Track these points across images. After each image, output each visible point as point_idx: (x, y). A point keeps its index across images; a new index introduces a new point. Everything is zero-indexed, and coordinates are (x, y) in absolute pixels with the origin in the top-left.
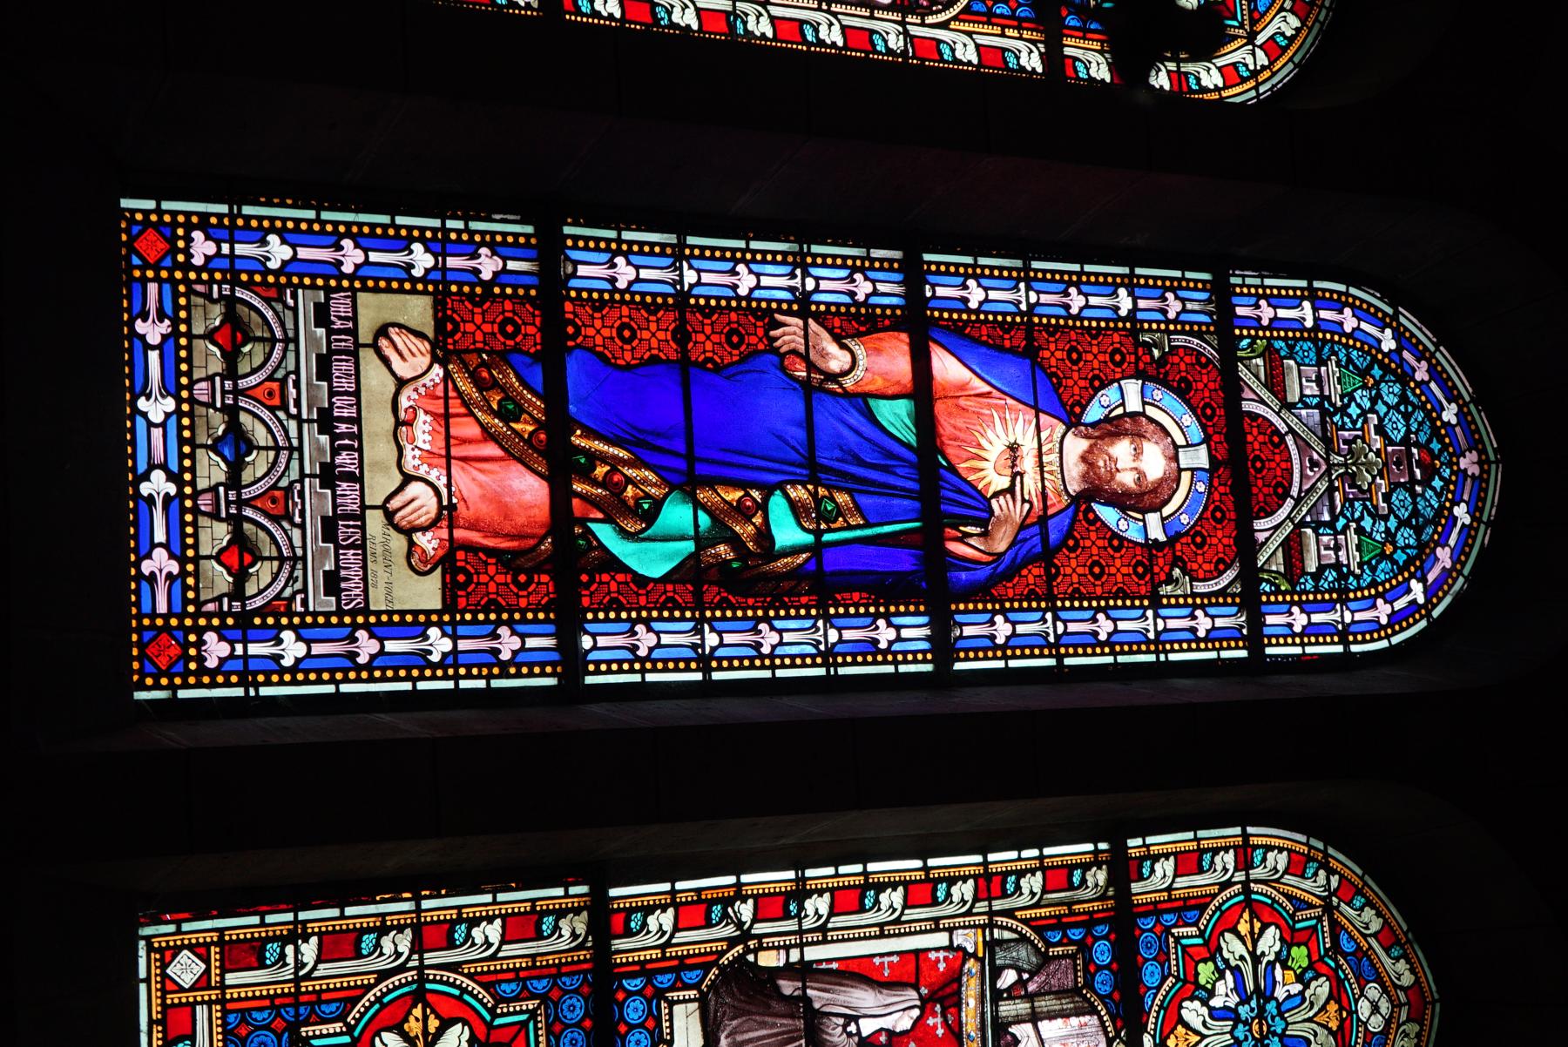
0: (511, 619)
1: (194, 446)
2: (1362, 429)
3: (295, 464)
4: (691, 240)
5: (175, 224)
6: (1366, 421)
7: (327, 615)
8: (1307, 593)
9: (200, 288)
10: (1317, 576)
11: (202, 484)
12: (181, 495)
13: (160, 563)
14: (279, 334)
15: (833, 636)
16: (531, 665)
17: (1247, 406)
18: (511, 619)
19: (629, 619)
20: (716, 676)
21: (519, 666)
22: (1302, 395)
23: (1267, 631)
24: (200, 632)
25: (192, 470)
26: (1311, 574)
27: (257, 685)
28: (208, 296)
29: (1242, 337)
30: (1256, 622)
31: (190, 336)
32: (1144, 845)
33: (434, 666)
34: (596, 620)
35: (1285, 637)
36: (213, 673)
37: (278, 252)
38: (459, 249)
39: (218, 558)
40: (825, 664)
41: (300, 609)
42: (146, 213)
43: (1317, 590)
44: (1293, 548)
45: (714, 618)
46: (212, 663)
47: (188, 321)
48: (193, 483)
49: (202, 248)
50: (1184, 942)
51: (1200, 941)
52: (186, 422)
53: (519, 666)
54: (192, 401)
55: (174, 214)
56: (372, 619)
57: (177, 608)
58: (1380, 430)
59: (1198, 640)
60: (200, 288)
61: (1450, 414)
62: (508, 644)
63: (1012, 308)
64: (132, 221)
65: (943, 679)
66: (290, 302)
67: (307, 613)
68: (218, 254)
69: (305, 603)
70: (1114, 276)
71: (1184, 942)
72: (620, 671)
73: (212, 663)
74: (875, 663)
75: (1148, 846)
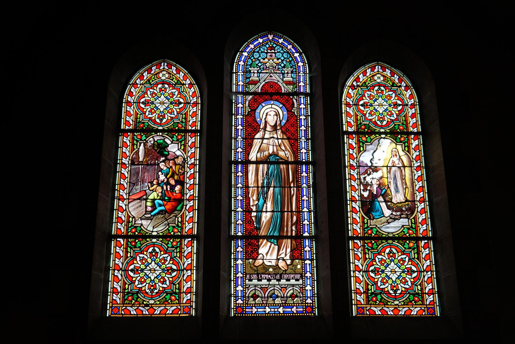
0: (302, 221)
1: (274, 303)
2: (264, 63)
3: (277, 286)
4: (233, 209)
5: (236, 306)
6: (262, 62)
7: (303, 281)
8: (296, 81)
9: (247, 302)
10: (293, 78)
11: (281, 302)
12: (283, 306)
13: (294, 309)
14: (254, 288)
15: (303, 138)
16: (309, 206)
17: (260, 91)
18: (302, 221)
19: (303, 252)
20: (309, 114)
21: (309, 208)
22: (257, 77)
23: (304, 92)
24: (306, 303)
25: (278, 304)
26: (293, 80)
27: (310, 185)
28: (248, 301)
29: (246, 90)
30: (302, 94)
31: (255, 304)
32: (350, 212)
33: (308, 175)
34: (300, 159)
35: (306, 110)
36: (313, 301)
37: (240, 288)
38: (237, 256)
39: (293, 300)
40: (310, 188)
41: (302, 286)
42: (234, 311)
43: (296, 78)
44: (288, 83)
45: (302, 209)
46: (311, 302)
47: (252, 304)
48: (280, 304)
49: (240, 301)
50: (364, 120)
51: (363, 117)
52: (270, 305)
53: (309, 208)
54: (266, 304)
55: (234, 306)
56: (303, 273)
57: (302, 307)
58: (264, 59)
59: (306, 108)
60: (247, 302)
61: (261, 40)
62: (307, 249)
63: (242, 142)
64: (236, 313)
65: (313, 163)
66: (248, 286)
67: (302, 284)
68: (241, 299)
69: (301, 285)
70: (235, 118)
71: (364, 120)
72: (309, 144)
73: (311, 302)
74: (308, 131)
75: (349, 179)
